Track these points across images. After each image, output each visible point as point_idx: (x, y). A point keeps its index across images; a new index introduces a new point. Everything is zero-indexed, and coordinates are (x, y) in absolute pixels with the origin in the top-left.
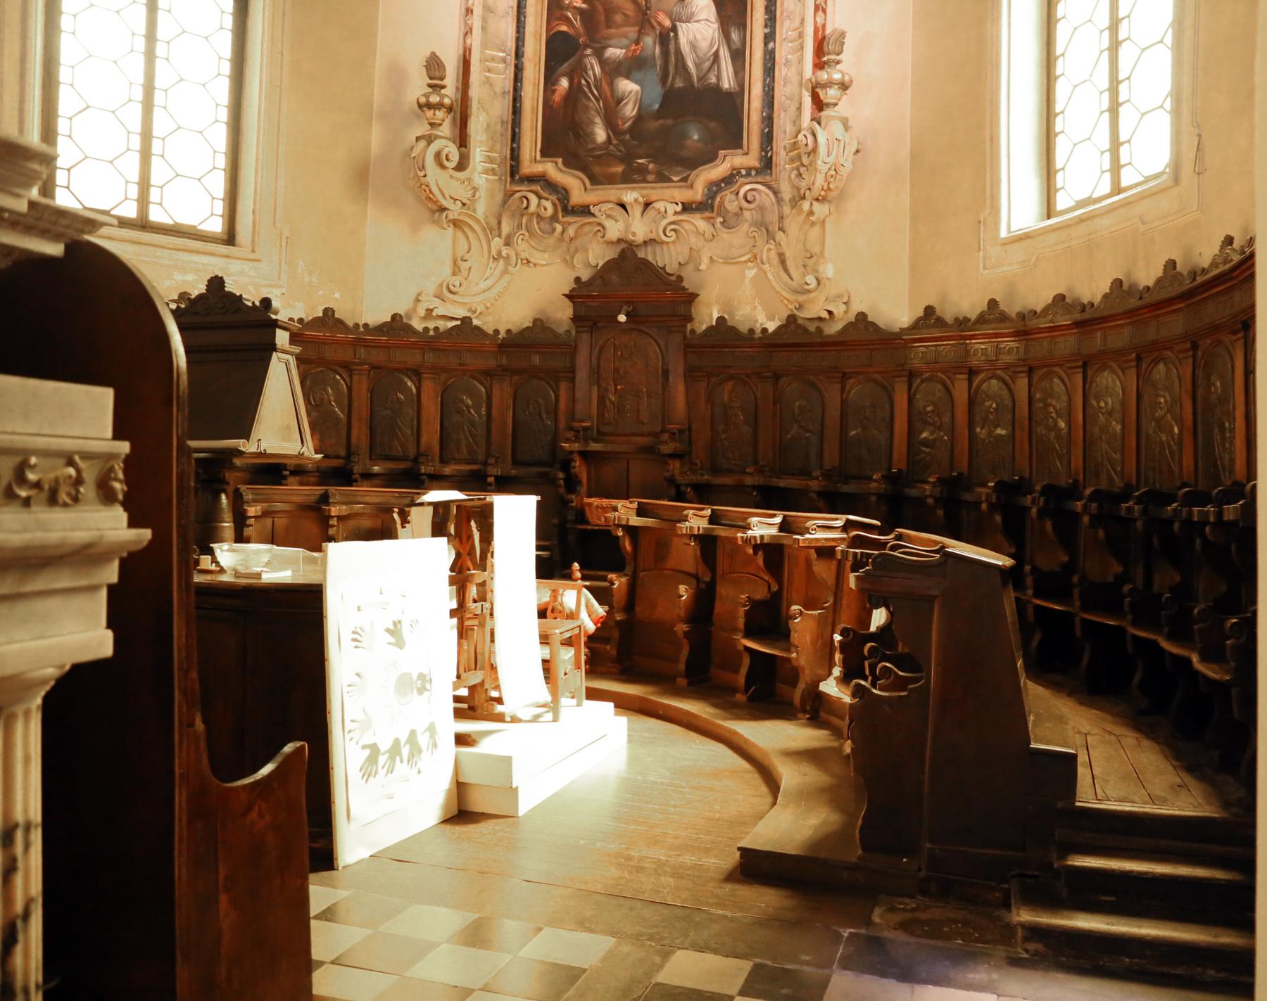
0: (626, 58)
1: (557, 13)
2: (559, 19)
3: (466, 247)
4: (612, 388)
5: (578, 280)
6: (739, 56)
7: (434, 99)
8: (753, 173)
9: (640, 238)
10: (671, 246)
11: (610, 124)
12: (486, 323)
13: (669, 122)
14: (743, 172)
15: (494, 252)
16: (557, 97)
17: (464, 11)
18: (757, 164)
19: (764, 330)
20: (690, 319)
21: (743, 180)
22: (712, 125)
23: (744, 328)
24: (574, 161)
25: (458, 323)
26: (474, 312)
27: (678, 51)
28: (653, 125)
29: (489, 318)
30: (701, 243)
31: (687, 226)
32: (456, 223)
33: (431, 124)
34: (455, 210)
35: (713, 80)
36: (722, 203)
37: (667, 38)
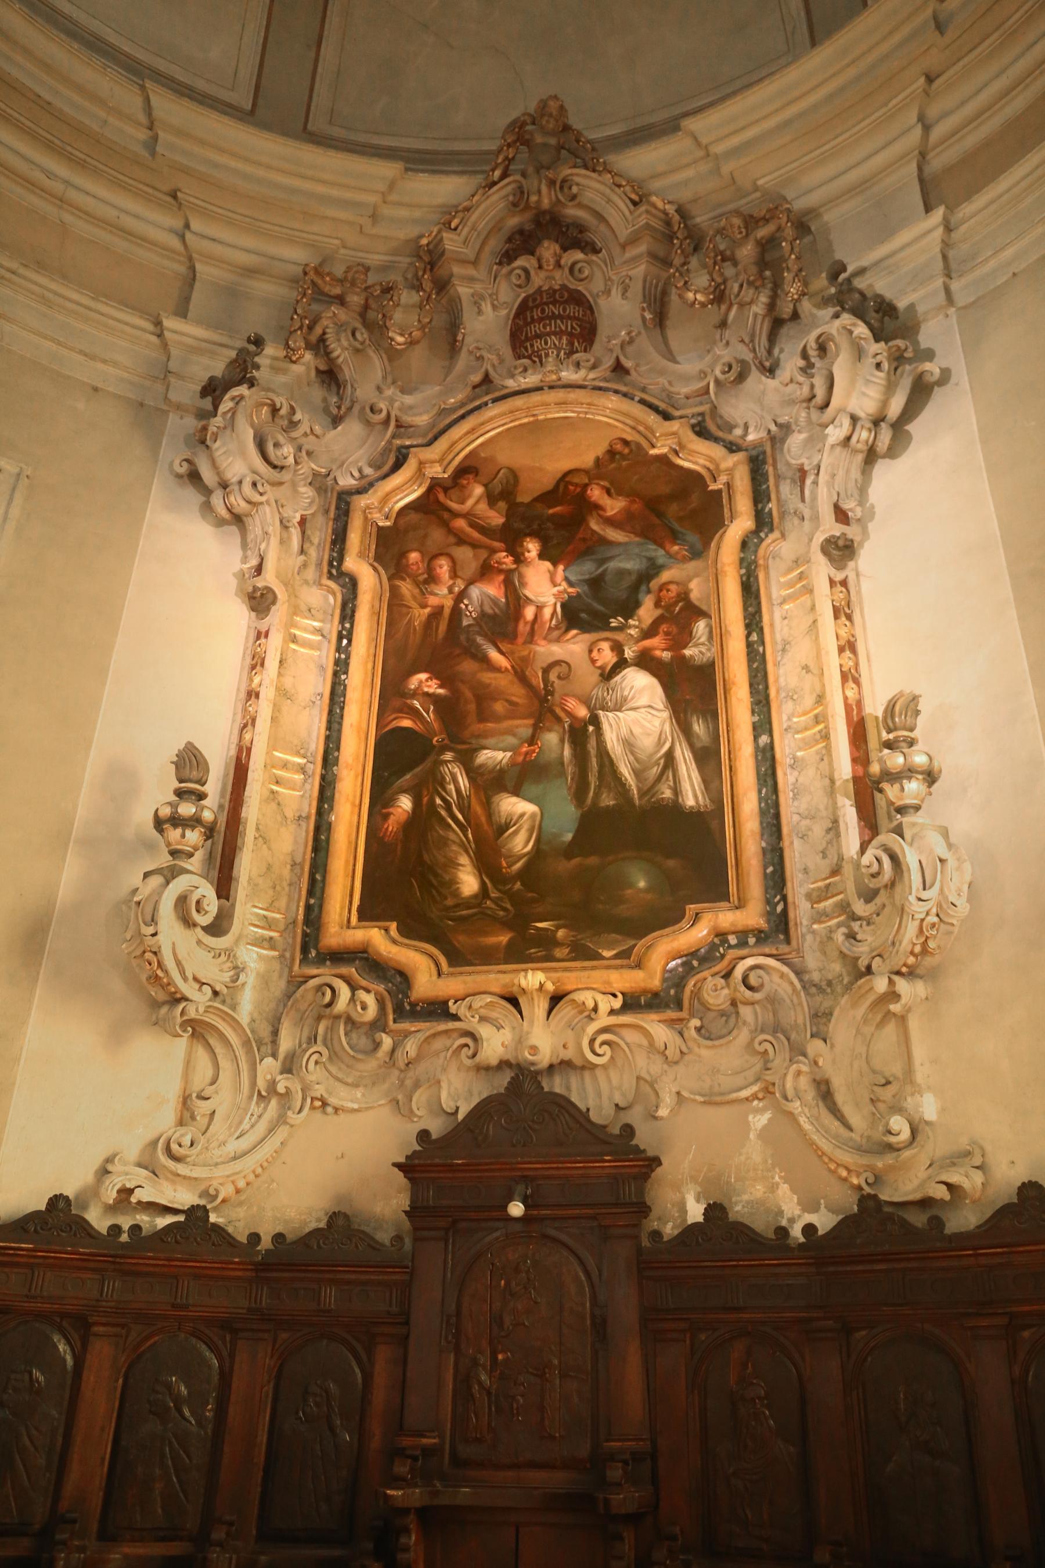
0: (512, 763)
1: (397, 703)
2: (401, 711)
3: (209, 1073)
4: (484, 1359)
5: (423, 1136)
6: (708, 758)
7: (187, 809)
8: (752, 941)
9: (545, 1057)
10: (599, 1072)
11: (487, 862)
12: (234, 1220)
13: (593, 860)
14: (733, 940)
15: (261, 1085)
16: (392, 825)
17: (243, 695)
18: (761, 923)
19: (809, 1229)
20: (643, 1210)
21: (732, 954)
22: (671, 863)
23: (761, 1225)
24: (417, 927)
25: (181, 1218)
26: (214, 1198)
27: (603, 753)
28: (564, 867)
29: (241, 1213)
30: (657, 1066)
31: (632, 1037)
32: (198, 1030)
33: (174, 853)
34: (199, 999)
35: (668, 794)
36: (696, 994)
37: (582, 734)
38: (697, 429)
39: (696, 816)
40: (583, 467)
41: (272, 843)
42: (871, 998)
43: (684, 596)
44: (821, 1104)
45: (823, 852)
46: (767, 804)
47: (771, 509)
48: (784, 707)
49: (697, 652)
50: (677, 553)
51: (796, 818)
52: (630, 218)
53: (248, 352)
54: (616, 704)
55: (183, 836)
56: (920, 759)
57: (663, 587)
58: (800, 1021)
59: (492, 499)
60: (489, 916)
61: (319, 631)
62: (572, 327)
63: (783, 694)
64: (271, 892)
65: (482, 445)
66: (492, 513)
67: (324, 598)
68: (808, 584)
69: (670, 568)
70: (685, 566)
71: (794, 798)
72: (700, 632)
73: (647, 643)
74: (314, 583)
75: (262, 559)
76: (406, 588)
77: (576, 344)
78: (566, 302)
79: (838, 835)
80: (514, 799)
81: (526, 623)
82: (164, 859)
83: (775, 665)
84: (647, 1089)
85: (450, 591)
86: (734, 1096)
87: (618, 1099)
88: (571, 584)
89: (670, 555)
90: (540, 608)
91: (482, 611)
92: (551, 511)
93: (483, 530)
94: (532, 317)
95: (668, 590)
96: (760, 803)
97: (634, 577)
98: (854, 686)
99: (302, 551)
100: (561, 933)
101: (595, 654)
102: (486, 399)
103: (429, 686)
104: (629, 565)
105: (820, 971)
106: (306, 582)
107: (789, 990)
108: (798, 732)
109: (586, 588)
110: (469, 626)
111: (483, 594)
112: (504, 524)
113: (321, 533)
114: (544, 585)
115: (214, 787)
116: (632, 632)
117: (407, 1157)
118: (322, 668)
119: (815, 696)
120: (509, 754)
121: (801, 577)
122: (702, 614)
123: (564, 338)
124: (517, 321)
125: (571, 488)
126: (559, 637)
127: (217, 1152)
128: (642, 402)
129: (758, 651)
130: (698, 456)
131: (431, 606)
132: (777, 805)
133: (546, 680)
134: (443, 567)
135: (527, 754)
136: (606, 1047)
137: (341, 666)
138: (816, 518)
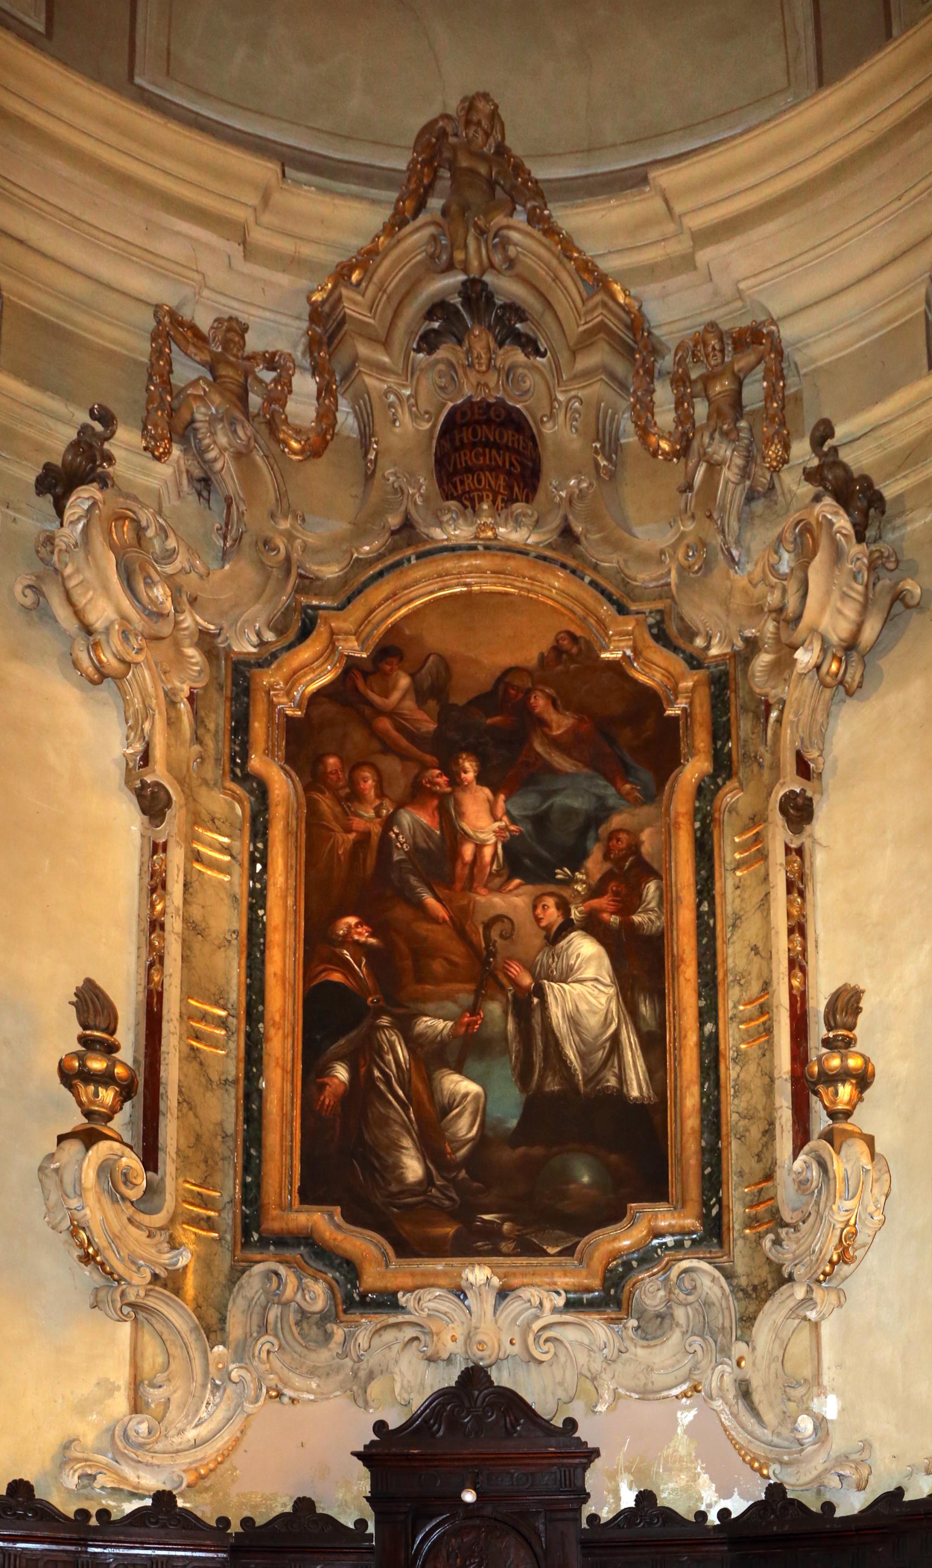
0: (454, 1033)
3: (160, 1360)
5: (380, 1426)
6: (655, 1045)
7: (97, 1065)
11: (432, 1145)
16: (328, 1098)
19: (724, 1514)
22: (614, 1158)
23: (684, 1509)
24: (360, 1214)
25: (148, 1502)
28: (508, 1155)
33: (88, 1114)
35: (613, 1082)
37: (528, 1005)
38: (655, 631)
39: (639, 1107)
40: (525, 664)
41: (197, 1106)
42: (791, 1304)
43: (635, 848)
44: (740, 1403)
45: (758, 1155)
46: (708, 1099)
47: (730, 749)
48: (731, 992)
49: (646, 920)
50: (628, 794)
51: (735, 1117)
52: (583, 310)
53: (94, 434)
54: (562, 974)
55: (96, 1094)
56: (854, 1063)
57: (613, 835)
58: (727, 1325)
59: (420, 694)
60: (435, 1205)
61: (225, 849)
62: (511, 464)
63: (730, 978)
64: (203, 1166)
65: (406, 617)
66: (421, 715)
67: (227, 803)
68: (763, 848)
69: (621, 812)
70: (637, 811)
71: (735, 1096)
72: (650, 895)
73: (595, 903)
74: (215, 784)
75: (148, 744)
76: (326, 803)
77: (516, 489)
78: (502, 424)
79: (773, 1138)
80: (456, 1077)
81: (464, 864)
82: (77, 1120)
83: (724, 942)
84: (589, 1385)
85: (378, 814)
86: (665, 1394)
87: (560, 1393)
88: (513, 821)
89: (622, 796)
90: (479, 847)
91: (415, 843)
92: (489, 721)
93: (412, 737)
94: (461, 440)
95: (618, 840)
96: (702, 1099)
97: (581, 819)
98: (800, 974)
99: (198, 739)
100: (506, 1227)
101: (539, 911)
102: (409, 552)
103: (360, 934)
104: (577, 803)
105: (748, 1276)
106: (205, 782)
107: (719, 1293)
108: (742, 1022)
109: (529, 827)
110: (401, 861)
111: (415, 821)
112: (435, 731)
113: (219, 718)
114: (484, 821)
115: (127, 1037)
116: (579, 888)
117: (365, 1446)
118: (235, 898)
119: (761, 982)
120: (450, 1024)
121: (758, 838)
122: (654, 874)
123: (502, 477)
124: (442, 441)
125: (513, 692)
126: (501, 886)
127: (177, 1440)
128: (593, 583)
129: (708, 924)
130: (655, 669)
131: (357, 831)
132: (717, 1102)
133: (487, 938)
134: (368, 784)
135: (469, 1025)
136: (549, 1344)
137: (258, 899)
138: (776, 767)
